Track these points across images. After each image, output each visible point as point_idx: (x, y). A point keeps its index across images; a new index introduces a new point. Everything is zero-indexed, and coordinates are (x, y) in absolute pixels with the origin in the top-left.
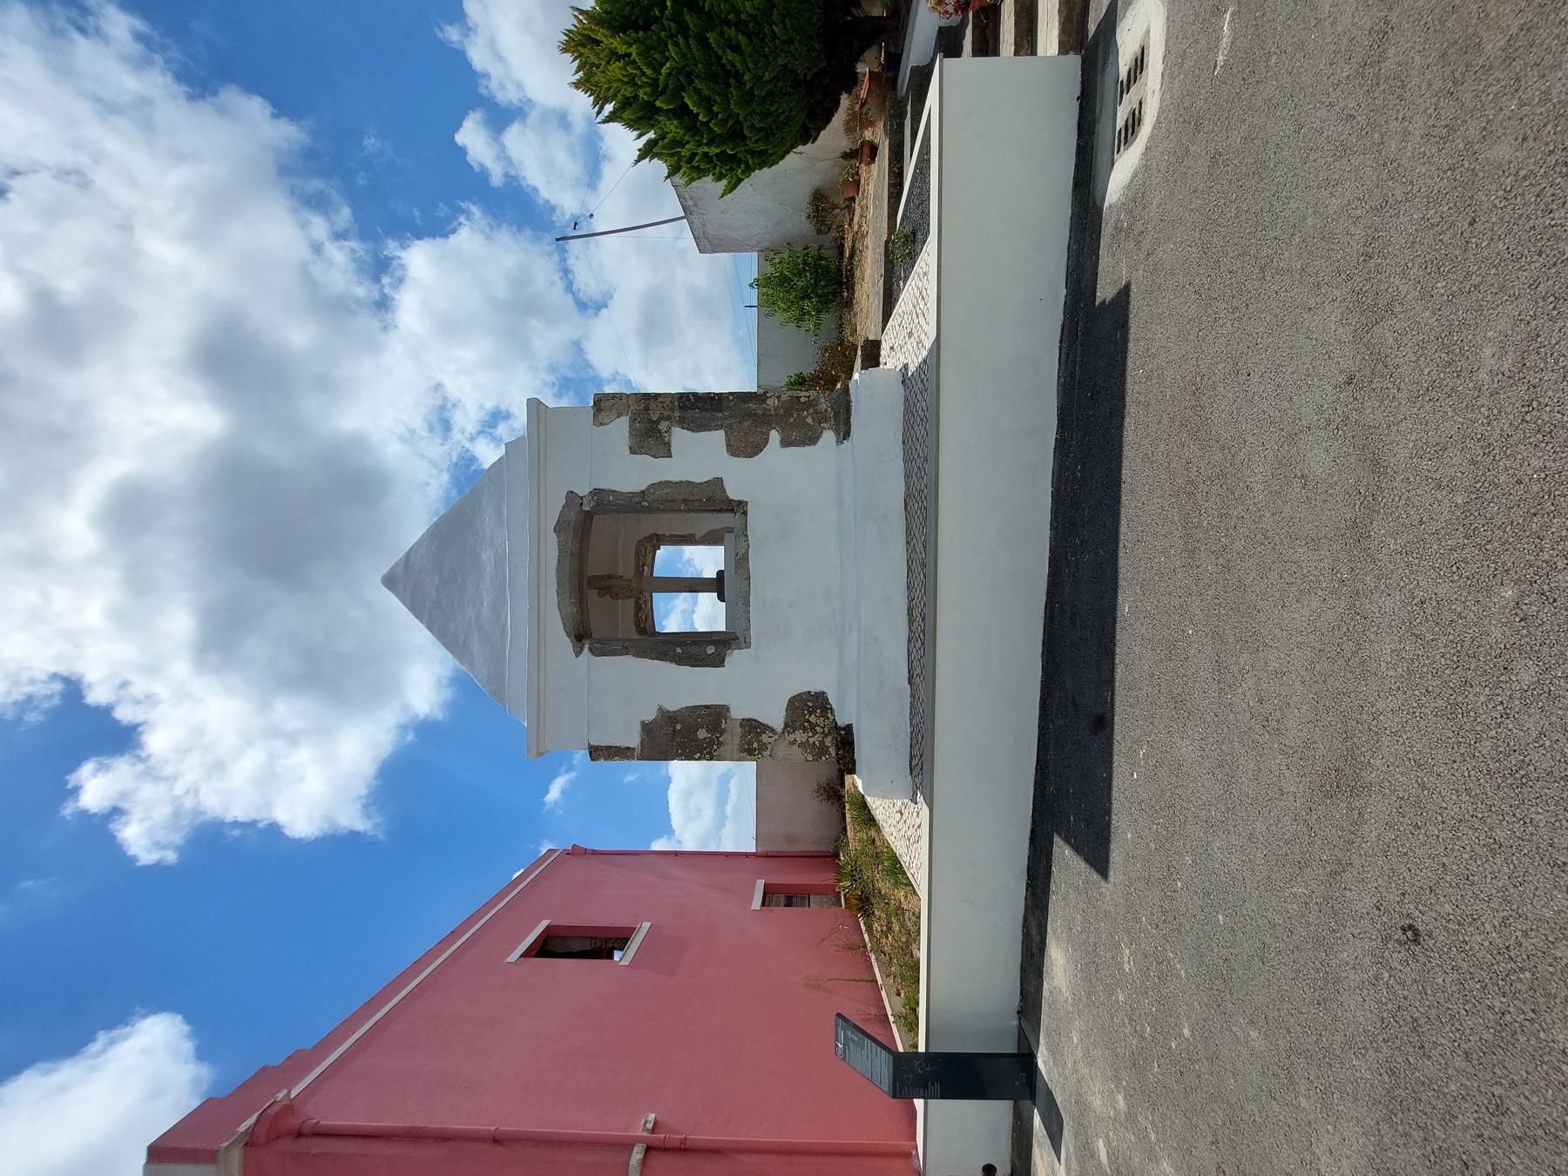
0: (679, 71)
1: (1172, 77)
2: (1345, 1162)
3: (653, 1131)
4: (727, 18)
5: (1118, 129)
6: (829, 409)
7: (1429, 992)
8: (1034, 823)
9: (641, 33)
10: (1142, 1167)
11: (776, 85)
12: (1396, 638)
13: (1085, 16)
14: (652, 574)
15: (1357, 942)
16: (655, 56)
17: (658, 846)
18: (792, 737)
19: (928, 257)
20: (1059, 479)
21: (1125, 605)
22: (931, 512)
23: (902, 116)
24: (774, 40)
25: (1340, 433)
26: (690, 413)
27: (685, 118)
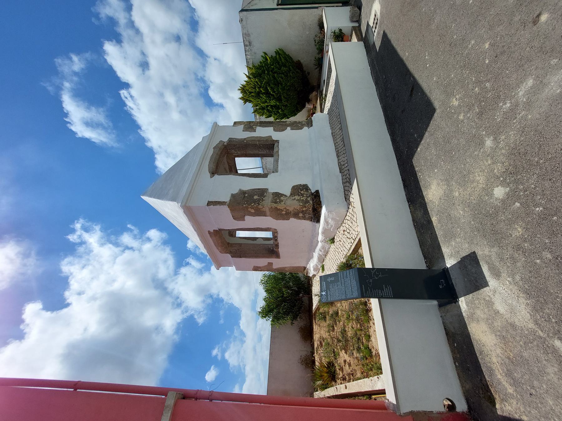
17: (236, 390)
18: (294, 198)
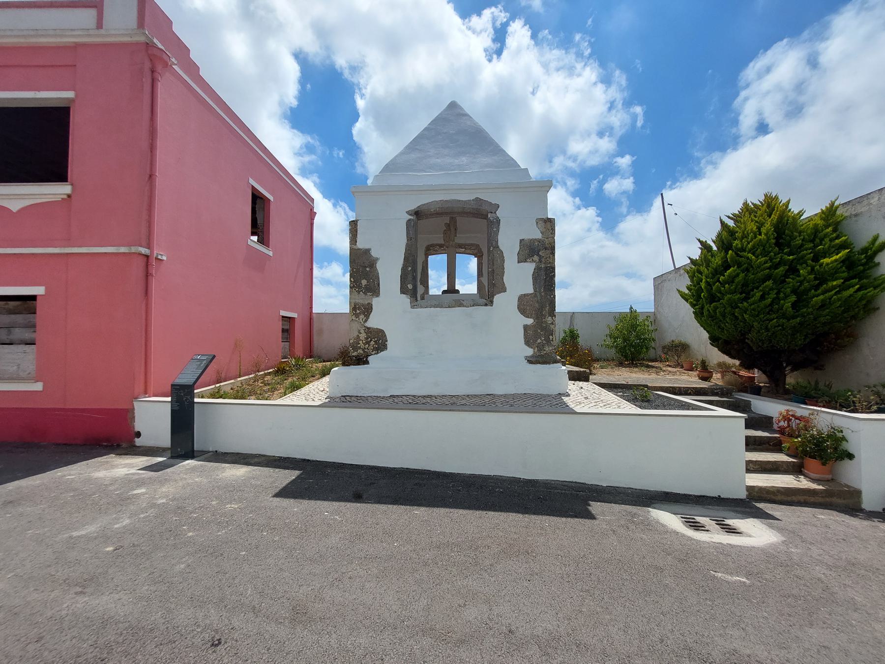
0: (750, 264)
1: (717, 548)
2: (114, 606)
3: (157, 259)
4: (782, 292)
5: (695, 517)
6: (545, 352)
7: (187, 649)
8: (313, 461)
9: (773, 241)
10: (128, 510)
11: (741, 321)
12: (367, 646)
13: (770, 501)
14: (457, 253)
15: (218, 618)
16: (759, 250)
18: (362, 331)
19: (629, 408)
20: (497, 479)
21: (420, 512)
22: (482, 408)
23: (722, 395)
24: (768, 320)
25: (484, 625)
26: (543, 273)
27: (722, 268)
